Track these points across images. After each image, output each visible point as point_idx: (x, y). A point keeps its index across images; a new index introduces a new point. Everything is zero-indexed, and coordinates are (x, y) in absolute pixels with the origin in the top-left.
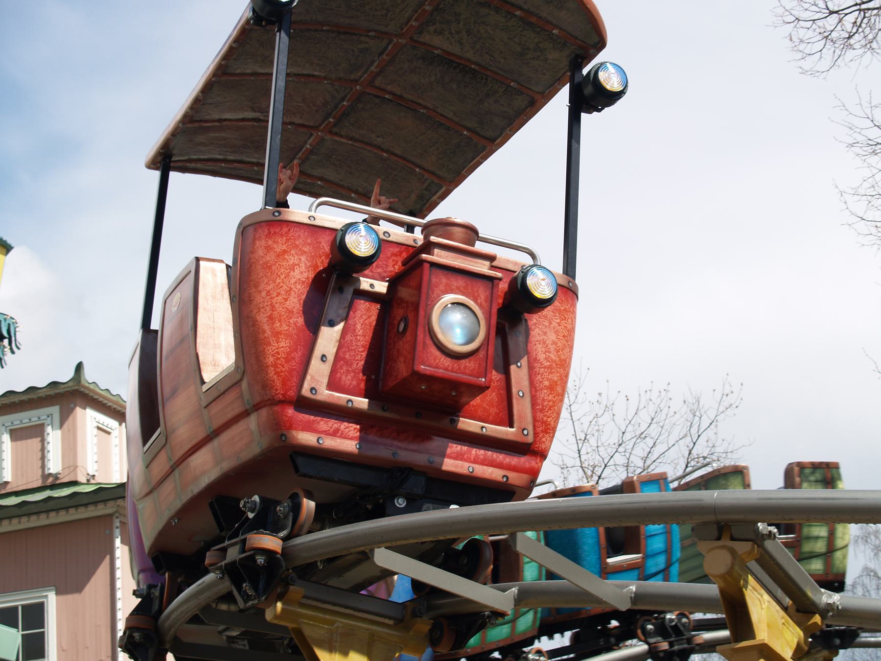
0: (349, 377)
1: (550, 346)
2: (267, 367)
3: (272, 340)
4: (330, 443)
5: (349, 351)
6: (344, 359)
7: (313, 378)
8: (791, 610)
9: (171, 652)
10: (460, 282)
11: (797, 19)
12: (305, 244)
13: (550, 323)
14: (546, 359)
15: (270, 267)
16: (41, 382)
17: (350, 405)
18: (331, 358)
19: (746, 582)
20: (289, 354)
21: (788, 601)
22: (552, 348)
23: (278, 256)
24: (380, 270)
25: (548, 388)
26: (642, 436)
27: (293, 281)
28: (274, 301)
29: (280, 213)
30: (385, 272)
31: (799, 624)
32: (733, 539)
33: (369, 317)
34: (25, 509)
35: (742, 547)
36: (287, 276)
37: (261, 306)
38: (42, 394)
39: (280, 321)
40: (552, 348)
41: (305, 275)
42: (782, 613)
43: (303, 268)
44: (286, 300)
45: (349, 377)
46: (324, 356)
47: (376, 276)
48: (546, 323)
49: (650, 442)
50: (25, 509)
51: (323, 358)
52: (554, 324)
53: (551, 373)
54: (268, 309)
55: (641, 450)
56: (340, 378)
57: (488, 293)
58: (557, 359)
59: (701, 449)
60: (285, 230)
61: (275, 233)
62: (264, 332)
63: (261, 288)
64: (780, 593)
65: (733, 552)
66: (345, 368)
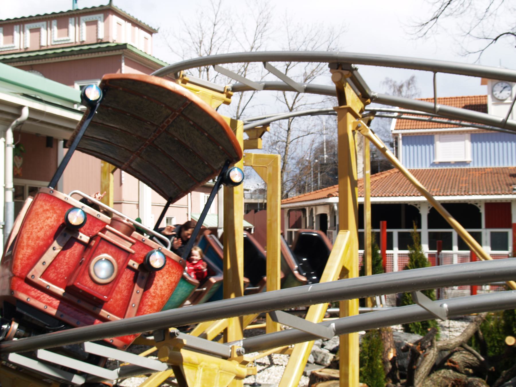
0: (54, 275)
1: (158, 287)
2: (18, 259)
3: (25, 248)
4: (33, 302)
5: (59, 263)
6: (55, 266)
7: (35, 271)
8: (361, 97)
9: (39, 349)
10: (113, 250)
12: (58, 209)
13: (163, 277)
14: (154, 292)
15: (38, 215)
16: (97, 5)
17: (48, 288)
18: (47, 264)
20: (30, 256)
21: (359, 94)
22: (159, 288)
23: (44, 211)
24: (89, 231)
25: (149, 305)
26: (312, 40)
27: (45, 224)
28: (33, 230)
29: (53, 192)
30: (91, 232)
31: (363, 102)
32: (342, 69)
33: (75, 250)
34: (90, 51)
35: (345, 73)
36: (44, 221)
37: (27, 230)
38: (97, 9)
39: (32, 240)
40: (159, 288)
41: (52, 223)
43: (53, 219)
44: (39, 232)
45: (54, 275)
46: (44, 262)
47: (86, 233)
48: (161, 276)
49: (314, 42)
50: (90, 51)
51: (44, 263)
52: (165, 277)
53: (154, 299)
54: (30, 233)
55: (311, 44)
56: (49, 274)
57: (125, 258)
58: (160, 294)
59: (332, 46)
60: (52, 200)
61: (47, 200)
62: (24, 243)
63: (31, 222)
65: (342, 74)
66: (53, 270)
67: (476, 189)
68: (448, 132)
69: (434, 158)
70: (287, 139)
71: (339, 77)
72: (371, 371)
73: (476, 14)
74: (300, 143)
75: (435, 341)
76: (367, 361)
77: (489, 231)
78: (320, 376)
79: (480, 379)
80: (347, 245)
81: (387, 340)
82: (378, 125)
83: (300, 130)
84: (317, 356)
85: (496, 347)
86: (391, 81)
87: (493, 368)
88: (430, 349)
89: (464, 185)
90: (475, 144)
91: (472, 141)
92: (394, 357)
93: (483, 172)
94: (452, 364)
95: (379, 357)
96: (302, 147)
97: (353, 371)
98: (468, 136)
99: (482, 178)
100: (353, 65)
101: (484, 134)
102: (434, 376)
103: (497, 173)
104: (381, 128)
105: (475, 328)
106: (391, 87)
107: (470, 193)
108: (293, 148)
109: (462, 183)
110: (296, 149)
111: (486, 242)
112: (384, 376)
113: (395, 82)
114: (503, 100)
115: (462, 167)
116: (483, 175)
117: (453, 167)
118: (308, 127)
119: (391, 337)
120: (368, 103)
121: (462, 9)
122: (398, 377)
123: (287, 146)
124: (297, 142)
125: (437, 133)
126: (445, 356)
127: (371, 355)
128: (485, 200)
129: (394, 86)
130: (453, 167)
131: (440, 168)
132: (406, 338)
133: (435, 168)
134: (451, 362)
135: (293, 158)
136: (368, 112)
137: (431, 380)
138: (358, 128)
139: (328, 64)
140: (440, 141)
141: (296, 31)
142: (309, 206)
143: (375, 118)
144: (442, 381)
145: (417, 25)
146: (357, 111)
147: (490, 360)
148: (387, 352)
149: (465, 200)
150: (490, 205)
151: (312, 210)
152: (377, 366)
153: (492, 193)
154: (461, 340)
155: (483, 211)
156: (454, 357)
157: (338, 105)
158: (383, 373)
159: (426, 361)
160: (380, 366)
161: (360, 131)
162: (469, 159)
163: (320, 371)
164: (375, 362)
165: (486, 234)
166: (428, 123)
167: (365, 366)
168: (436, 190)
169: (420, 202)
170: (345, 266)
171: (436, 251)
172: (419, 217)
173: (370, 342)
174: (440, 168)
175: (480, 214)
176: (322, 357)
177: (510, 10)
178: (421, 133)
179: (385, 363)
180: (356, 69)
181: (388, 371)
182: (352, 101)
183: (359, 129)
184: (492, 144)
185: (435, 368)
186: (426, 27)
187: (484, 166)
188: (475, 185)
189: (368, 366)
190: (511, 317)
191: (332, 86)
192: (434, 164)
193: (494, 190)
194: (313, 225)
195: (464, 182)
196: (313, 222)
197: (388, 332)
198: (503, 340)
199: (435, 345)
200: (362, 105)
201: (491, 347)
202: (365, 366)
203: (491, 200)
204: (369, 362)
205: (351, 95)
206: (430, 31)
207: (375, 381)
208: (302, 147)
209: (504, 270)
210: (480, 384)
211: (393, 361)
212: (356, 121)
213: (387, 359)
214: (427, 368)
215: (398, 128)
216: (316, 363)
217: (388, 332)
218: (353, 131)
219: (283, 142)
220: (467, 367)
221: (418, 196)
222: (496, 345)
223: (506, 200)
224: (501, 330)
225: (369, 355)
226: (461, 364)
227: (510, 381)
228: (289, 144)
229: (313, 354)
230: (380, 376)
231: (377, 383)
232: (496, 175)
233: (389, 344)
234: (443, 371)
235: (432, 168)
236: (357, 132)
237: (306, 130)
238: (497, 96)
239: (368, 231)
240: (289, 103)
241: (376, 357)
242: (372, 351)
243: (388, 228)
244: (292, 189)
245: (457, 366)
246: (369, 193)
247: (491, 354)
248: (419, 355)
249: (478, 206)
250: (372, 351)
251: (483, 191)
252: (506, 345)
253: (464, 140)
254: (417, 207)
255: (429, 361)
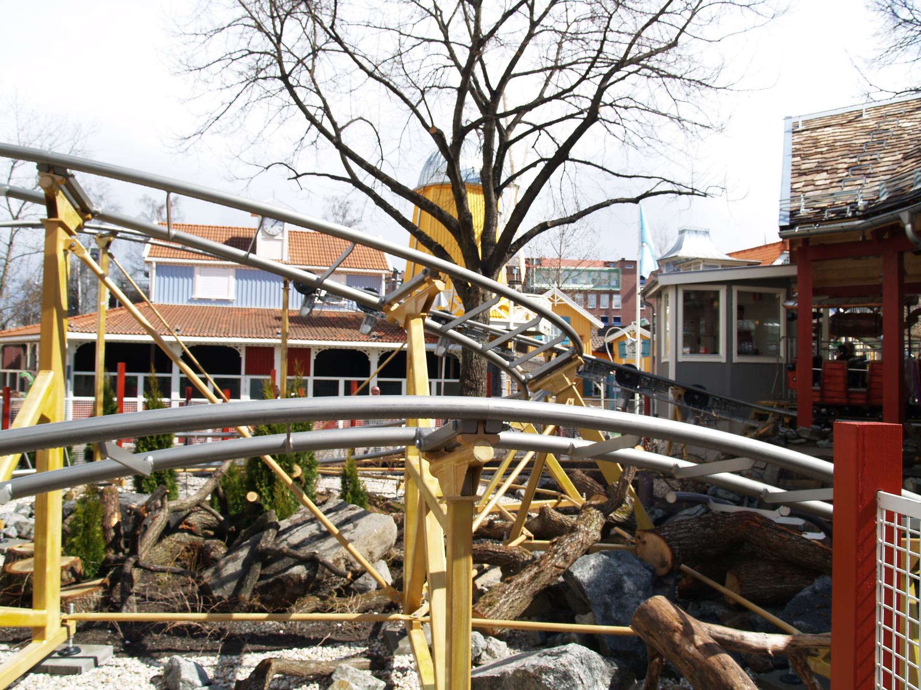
8: (79, 211)
11: (611, 15)
19: (58, 193)
21: (78, 206)
26: (51, 135)
31: (81, 216)
32: (55, 173)
35: (58, 178)
42: (74, 210)
49: (54, 138)
55: (50, 140)
59: (78, 147)
64: (74, 202)
65: (53, 179)
67: (237, 331)
68: (210, 265)
69: (192, 294)
70: (8, 255)
71: (48, 181)
72: (86, 541)
73: (247, 137)
74: (25, 262)
75: (166, 501)
76: (82, 529)
77: (249, 377)
78: (19, 552)
79: (219, 541)
80: (48, 388)
81: (111, 503)
82: (131, 249)
83: (26, 246)
84: (22, 528)
85: (238, 504)
86: (150, 199)
87: (233, 527)
88: (160, 510)
89: (224, 326)
90: (240, 281)
91: (237, 278)
92: (118, 523)
93: (247, 313)
94: (188, 527)
95: (97, 524)
96: (28, 267)
97: (53, 543)
98: (233, 271)
99: (244, 319)
100: (68, 170)
101: (245, 270)
102: (166, 542)
103: (262, 315)
104: (134, 254)
105: (214, 484)
106: (149, 206)
107: (230, 335)
108: (15, 268)
109: (222, 323)
110: (19, 269)
111: (245, 390)
112: (103, 546)
113: (155, 201)
114: (274, 236)
115: (224, 306)
116: (247, 316)
117: (214, 305)
118: (37, 243)
119: (116, 499)
120: (88, 219)
121: (231, 129)
122: (122, 546)
123: (7, 264)
124: (22, 260)
125: (197, 265)
126: (181, 517)
127: (86, 522)
128: (246, 344)
129: (153, 205)
130: (214, 305)
131: (199, 305)
132: (135, 499)
133: (193, 304)
134: (187, 524)
135: (14, 281)
136: (107, 232)
137: (163, 546)
138: (71, 247)
139: (35, 164)
140: (201, 274)
141: (30, 121)
142: (31, 342)
143: (116, 239)
144: (175, 546)
145: (178, 137)
146: (73, 228)
147: (230, 520)
148: (110, 517)
149: (223, 343)
150: (252, 350)
151: (35, 346)
152: (94, 534)
153: (254, 336)
154: (199, 498)
155: (243, 355)
156: (191, 518)
157: (46, 217)
158: (102, 542)
159: (155, 525)
160: (98, 535)
161: (73, 251)
162: (232, 296)
163: (20, 547)
164: (92, 529)
165: (246, 381)
166: (182, 252)
167: (78, 535)
168: (191, 330)
169: (275, 345)
170: (45, 414)
171: (185, 399)
172: (367, 364)
173: (86, 506)
174: (199, 305)
175: (240, 359)
176: (28, 530)
177: (285, 138)
178: (179, 264)
179: (105, 530)
180: (73, 176)
181: (111, 539)
182: (66, 215)
183: (73, 249)
184: (268, 283)
185: (168, 530)
186: (187, 141)
187: (249, 306)
188: (237, 327)
189: (83, 535)
190: (254, 471)
191: (41, 192)
192: (192, 300)
193: (257, 333)
194: (35, 365)
195: (224, 322)
196: (36, 362)
197: (112, 493)
198: (245, 497)
199: (166, 506)
200: (81, 221)
201: (234, 504)
202: (78, 535)
203: (252, 344)
204: (84, 530)
205: (64, 207)
206: (192, 147)
207: (92, 553)
208: (28, 267)
209: (188, 418)
210: (217, 546)
211: (117, 528)
212: (69, 238)
213: (109, 525)
214: (156, 533)
215: (152, 255)
216: (19, 537)
217: (112, 493)
218: (65, 251)
219: (610, 277)
220: (205, 528)
221: (143, 334)
222: (239, 502)
223: (269, 344)
224: (244, 486)
225: (84, 522)
226: (198, 525)
227: (248, 541)
228: (10, 262)
229: (16, 527)
230: (99, 546)
231: (94, 555)
232: (261, 317)
233: (113, 507)
234: (176, 535)
235: (189, 304)
236: (69, 251)
237: (34, 246)
238: (267, 231)
239: (100, 375)
240: (13, 210)
241: (94, 524)
242: (89, 516)
243: (127, 371)
244: (12, 318)
245: (193, 528)
246: (103, 328)
247: (233, 512)
248: (144, 518)
249: (238, 350)
250: (89, 516)
251: (245, 333)
252: (248, 502)
253: (228, 275)
254: (367, 353)
255: (158, 524)
